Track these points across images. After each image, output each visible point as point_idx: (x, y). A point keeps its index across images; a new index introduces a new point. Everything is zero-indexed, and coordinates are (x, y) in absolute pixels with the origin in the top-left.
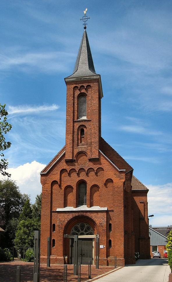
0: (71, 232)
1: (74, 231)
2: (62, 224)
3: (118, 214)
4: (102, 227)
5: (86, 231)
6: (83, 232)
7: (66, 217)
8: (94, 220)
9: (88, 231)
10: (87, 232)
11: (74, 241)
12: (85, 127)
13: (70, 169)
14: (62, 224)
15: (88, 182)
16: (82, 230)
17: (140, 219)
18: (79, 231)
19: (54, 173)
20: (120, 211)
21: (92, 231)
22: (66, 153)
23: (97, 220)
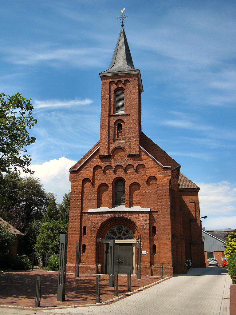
0: (106, 236)
3: (163, 216)
6: (121, 235)
9: (126, 235)
12: (123, 122)
13: (105, 166)
16: (120, 233)
18: (115, 235)
22: (101, 149)
23: (137, 222)
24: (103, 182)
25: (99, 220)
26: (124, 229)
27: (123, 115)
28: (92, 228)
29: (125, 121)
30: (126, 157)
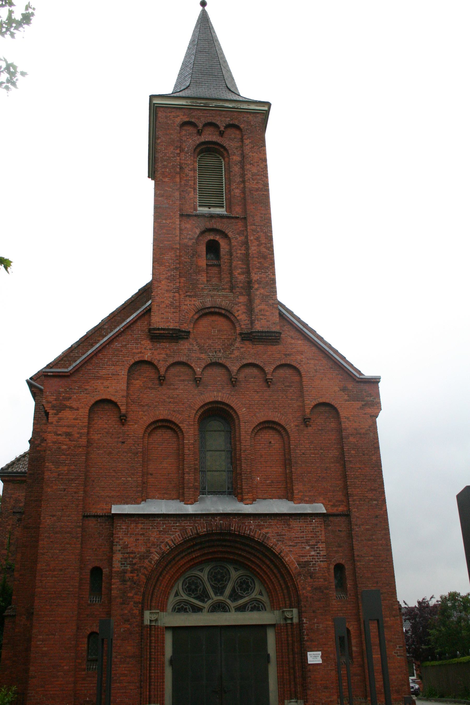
0: (172, 600)
1: (185, 597)
2: (136, 567)
3: (368, 530)
4: (309, 580)
5: (234, 596)
6: (224, 598)
7: (154, 536)
8: (277, 550)
9: (242, 597)
10: (241, 602)
11: (292, 609)
12: (225, 235)
13: (168, 364)
14: (136, 567)
15: (242, 412)
16: (219, 591)
17: (245, 218)
18: (203, 596)
19: (103, 372)
20: (377, 517)
21: (261, 594)
22: (155, 308)
23: (286, 549)
24: (163, 413)
25: (153, 544)
26: (234, 574)
27: (221, 217)
28: (125, 572)
29: (230, 234)
30: (239, 340)
